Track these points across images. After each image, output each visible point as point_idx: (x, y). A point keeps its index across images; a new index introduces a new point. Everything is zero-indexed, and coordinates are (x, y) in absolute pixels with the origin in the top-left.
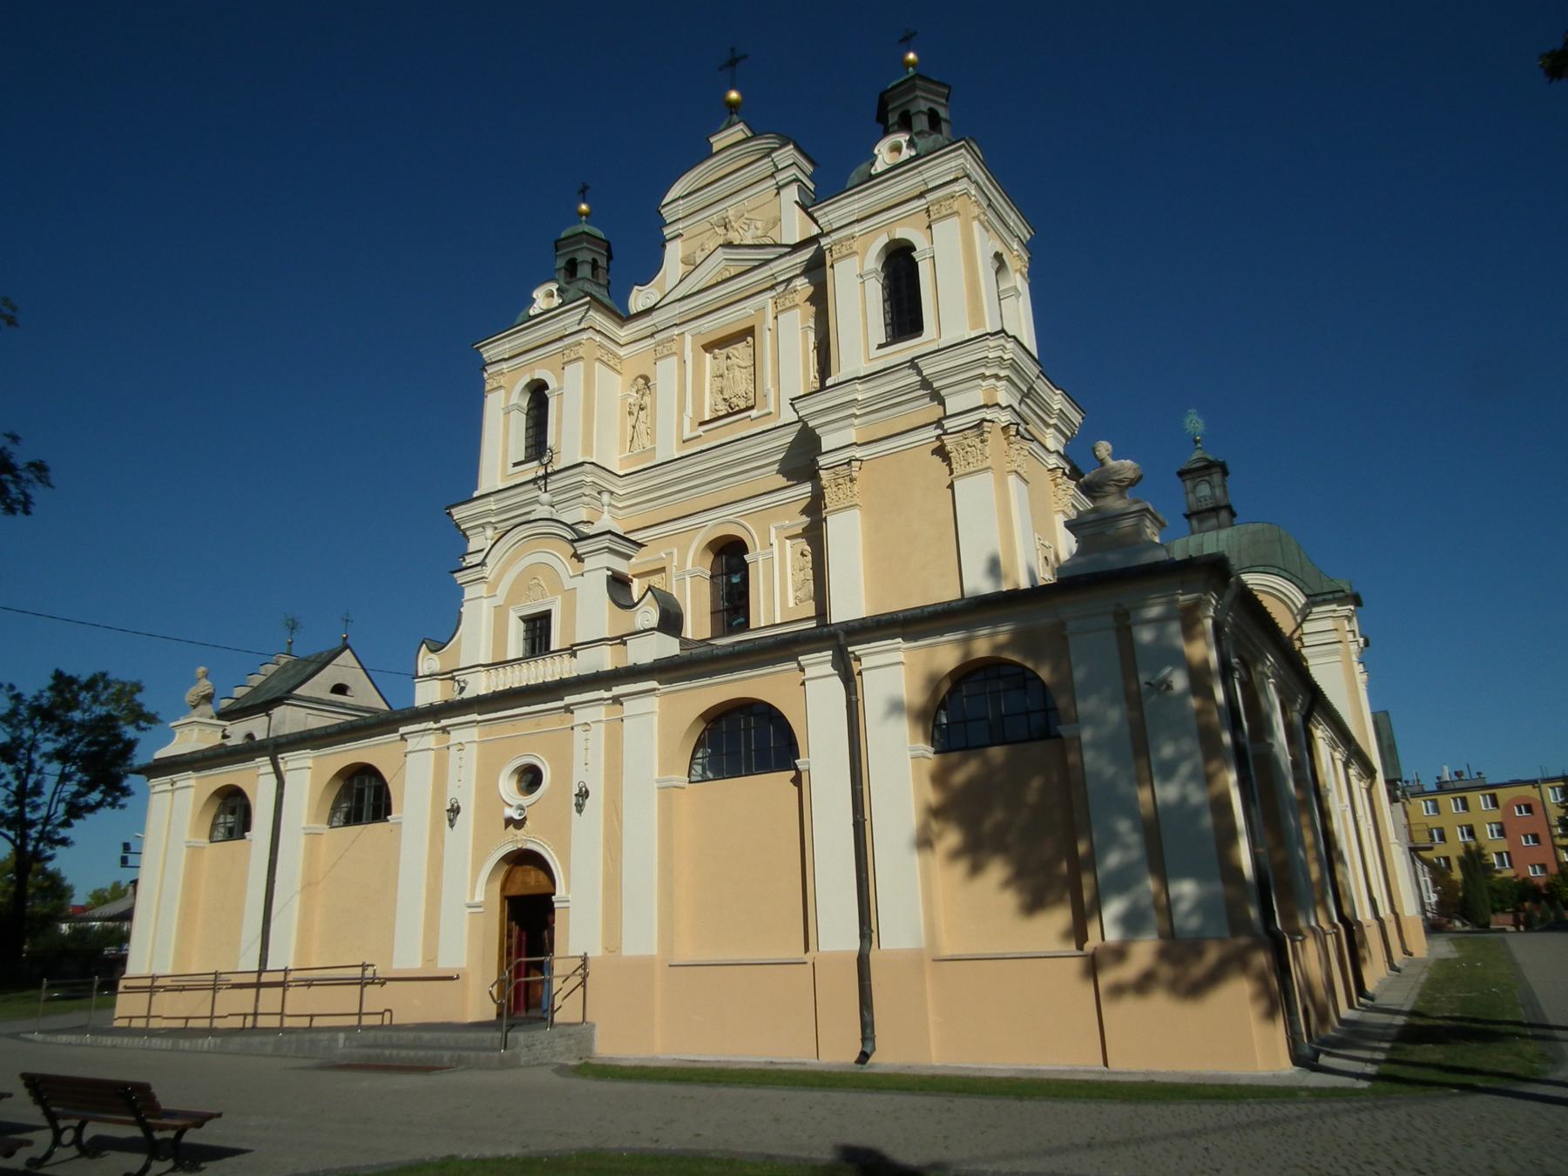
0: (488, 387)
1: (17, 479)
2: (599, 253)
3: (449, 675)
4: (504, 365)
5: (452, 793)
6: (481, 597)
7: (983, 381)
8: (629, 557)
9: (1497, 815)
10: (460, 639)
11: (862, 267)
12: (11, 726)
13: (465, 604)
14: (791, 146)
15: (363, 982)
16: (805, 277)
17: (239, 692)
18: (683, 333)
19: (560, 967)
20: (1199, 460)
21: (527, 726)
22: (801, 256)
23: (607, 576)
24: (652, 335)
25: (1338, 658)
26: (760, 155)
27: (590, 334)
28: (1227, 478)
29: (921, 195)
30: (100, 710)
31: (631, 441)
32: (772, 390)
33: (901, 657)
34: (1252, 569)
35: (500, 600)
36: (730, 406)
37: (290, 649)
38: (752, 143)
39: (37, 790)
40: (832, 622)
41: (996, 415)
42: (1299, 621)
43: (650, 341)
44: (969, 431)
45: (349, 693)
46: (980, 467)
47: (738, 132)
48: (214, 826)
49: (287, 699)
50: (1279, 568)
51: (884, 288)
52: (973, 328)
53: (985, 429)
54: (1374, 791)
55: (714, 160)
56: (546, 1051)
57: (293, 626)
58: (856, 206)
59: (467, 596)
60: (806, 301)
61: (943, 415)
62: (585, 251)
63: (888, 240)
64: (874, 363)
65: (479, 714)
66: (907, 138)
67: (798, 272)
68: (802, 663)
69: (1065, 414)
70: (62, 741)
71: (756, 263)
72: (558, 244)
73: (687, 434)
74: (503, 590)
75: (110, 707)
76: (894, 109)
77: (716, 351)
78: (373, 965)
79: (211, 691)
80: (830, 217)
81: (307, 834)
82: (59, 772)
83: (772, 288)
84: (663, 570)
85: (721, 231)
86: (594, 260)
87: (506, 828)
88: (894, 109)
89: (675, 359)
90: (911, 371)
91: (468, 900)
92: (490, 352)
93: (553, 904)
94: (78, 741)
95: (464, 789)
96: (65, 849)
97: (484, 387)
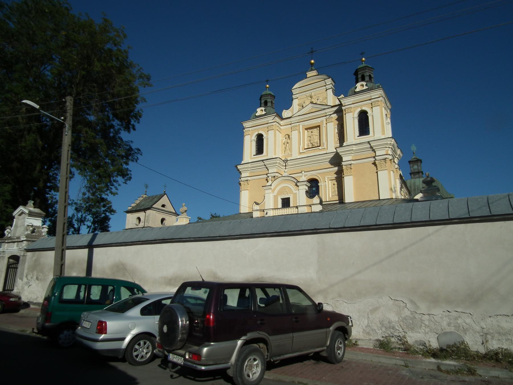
2: (272, 99)
14: (331, 79)
17: (133, 205)
18: (299, 125)
20: (415, 158)
22: (333, 109)
24: (291, 124)
28: (421, 164)
29: (370, 100)
32: (325, 142)
36: (313, 145)
37: (146, 193)
40: (346, 202)
41: (389, 157)
45: (165, 207)
47: (314, 73)
49: (151, 208)
55: (308, 79)
57: (147, 187)
60: (335, 120)
61: (375, 156)
66: (366, 83)
67: (332, 113)
72: (262, 96)
77: (308, 130)
80: (345, 102)
83: (326, 116)
85: (310, 98)
88: (360, 74)
90: (368, 144)
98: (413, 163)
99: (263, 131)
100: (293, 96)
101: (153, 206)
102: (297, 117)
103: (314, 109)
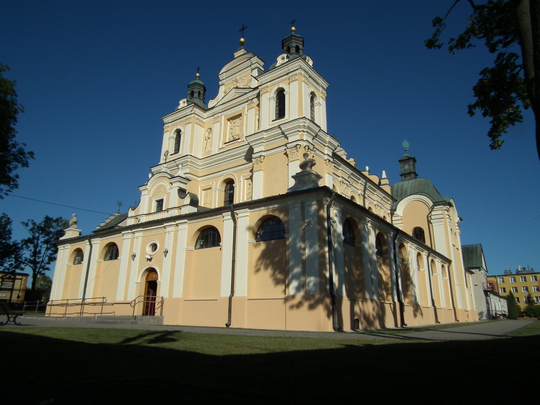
0: (165, 131)
1: (25, 157)
3: (136, 217)
4: (170, 124)
5: (135, 251)
6: (146, 195)
7: (299, 132)
8: (186, 184)
9: (536, 284)
10: (139, 207)
11: (270, 96)
12: (33, 232)
13: (142, 196)
14: (256, 57)
15: (103, 304)
16: (257, 98)
17: (102, 224)
18: (222, 115)
19: (158, 300)
20: (405, 157)
21: (154, 232)
22: (256, 92)
23: (178, 189)
24: (213, 116)
25: (442, 223)
26: (246, 60)
27: (194, 115)
29: (288, 74)
30: (59, 228)
31: (205, 148)
33: (248, 214)
34: (418, 193)
35: (151, 196)
37: (119, 212)
38: (245, 56)
39: (40, 252)
41: (302, 143)
42: (430, 211)
43: (212, 117)
44: (294, 148)
46: (296, 159)
47: (242, 51)
48: (75, 260)
50: (426, 193)
51: (276, 102)
52: (299, 116)
53: (298, 147)
54: (450, 267)
55: (235, 60)
56: (147, 322)
57: (120, 204)
58: (269, 77)
59: (142, 194)
60: (257, 106)
62: (196, 89)
63: (277, 88)
64: (270, 126)
65: (142, 228)
66: (286, 55)
67: (255, 97)
68: (223, 215)
69: (331, 143)
70: (47, 238)
71: (243, 94)
73: (221, 147)
74: (152, 193)
75: (61, 228)
76: (286, 46)
77: (231, 121)
78: (106, 298)
79: (76, 221)
81: (97, 262)
82: (46, 247)
83: (247, 101)
84: (210, 188)
86: (199, 92)
87: (147, 261)
88: (286, 46)
89: (219, 123)
91: (136, 282)
92: (166, 120)
93: (157, 283)
94: (52, 238)
95: (137, 251)
96: (48, 271)
97: (164, 131)
98: (404, 163)
99: (181, 126)
100: (219, 82)
101: (118, 225)
102: (220, 106)
103: (237, 95)
